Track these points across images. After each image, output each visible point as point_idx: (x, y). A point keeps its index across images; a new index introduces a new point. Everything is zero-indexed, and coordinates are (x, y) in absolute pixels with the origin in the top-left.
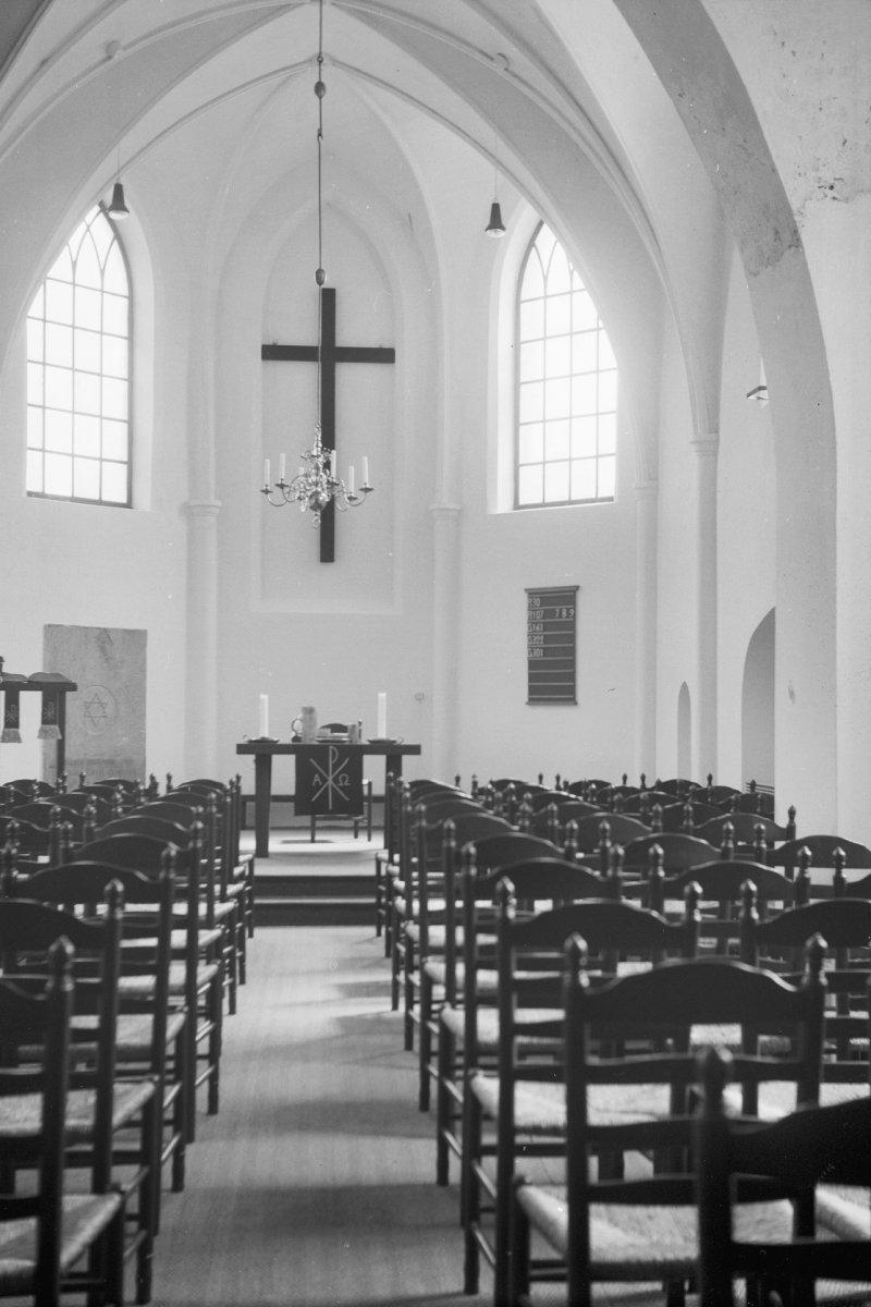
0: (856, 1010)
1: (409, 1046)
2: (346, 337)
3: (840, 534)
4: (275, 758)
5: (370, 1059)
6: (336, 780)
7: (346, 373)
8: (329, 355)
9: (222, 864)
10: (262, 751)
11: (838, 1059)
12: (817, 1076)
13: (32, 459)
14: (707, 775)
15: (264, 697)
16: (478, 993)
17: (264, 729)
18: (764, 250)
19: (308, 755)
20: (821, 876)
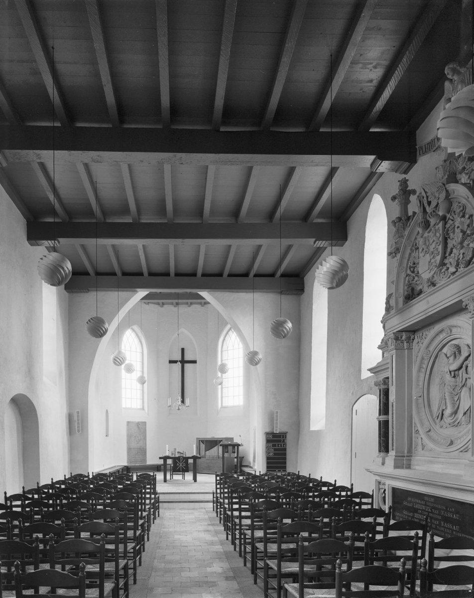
0: (365, 517)
1: (220, 523)
2: (187, 358)
3: (236, 155)
4: (168, 460)
5: (213, 525)
6: (182, 465)
7: (187, 366)
8: (183, 362)
9: (83, 492)
10: (165, 458)
11: (338, 573)
12: (362, 511)
13: (123, 400)
14: (36, 483)
15: (167, 445)
16: (14, 592)
17: (167, 454)
18: (416, 515)
19: (176, 460)
20: (343, 494)
